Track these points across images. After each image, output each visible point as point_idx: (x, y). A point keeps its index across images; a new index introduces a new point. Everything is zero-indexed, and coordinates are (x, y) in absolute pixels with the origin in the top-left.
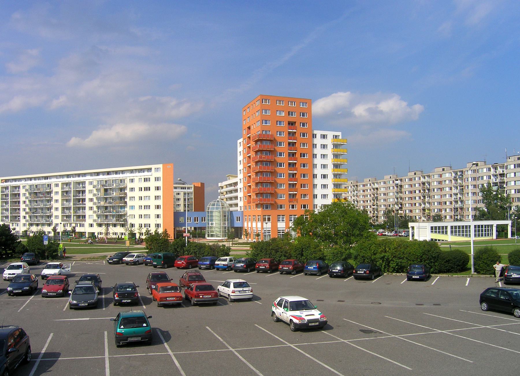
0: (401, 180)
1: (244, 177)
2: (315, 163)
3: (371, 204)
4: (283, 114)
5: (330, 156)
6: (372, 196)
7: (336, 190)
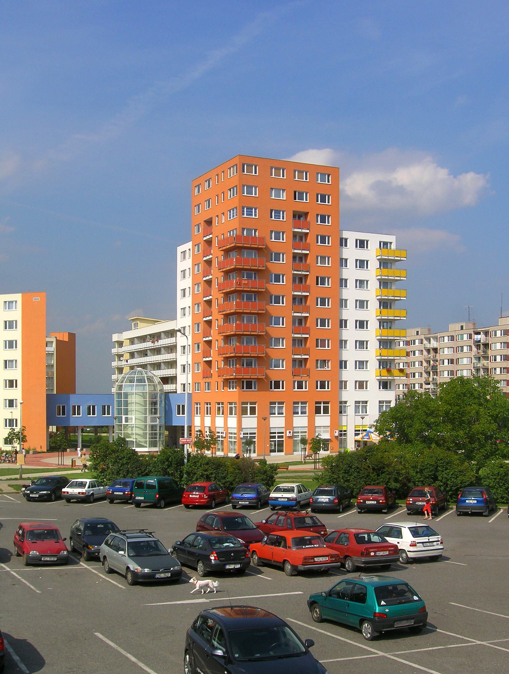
0: (486, 333)
1: (194, 324)
2: (344, 297)
3: (423, 380)
4: (283, 196)
5: (373, 285)
6: (425, 364)
7: (385, 352)
